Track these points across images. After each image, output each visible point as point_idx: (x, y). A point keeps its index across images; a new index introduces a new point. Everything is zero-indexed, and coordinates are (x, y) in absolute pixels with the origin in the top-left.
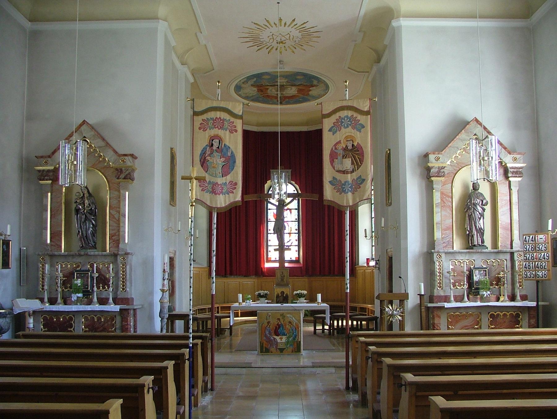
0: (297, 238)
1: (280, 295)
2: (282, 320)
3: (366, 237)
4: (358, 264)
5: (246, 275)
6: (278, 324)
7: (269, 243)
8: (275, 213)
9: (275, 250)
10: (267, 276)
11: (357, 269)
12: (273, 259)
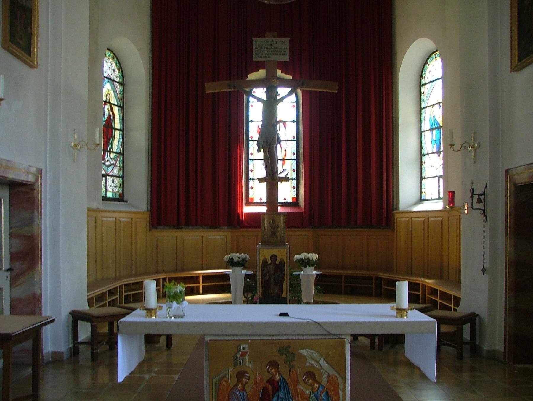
0: (295, 167)
1: (269, 262)
2: (283, 369)
3: (452, 145)
4: (397, 208)
5: (214, 225)
6: (271, 381)
7: (251, 175)
8: (260, 127)
9: (261, 180)
10: (248, 227)
11: (397, 216)
12: (256, 200)
